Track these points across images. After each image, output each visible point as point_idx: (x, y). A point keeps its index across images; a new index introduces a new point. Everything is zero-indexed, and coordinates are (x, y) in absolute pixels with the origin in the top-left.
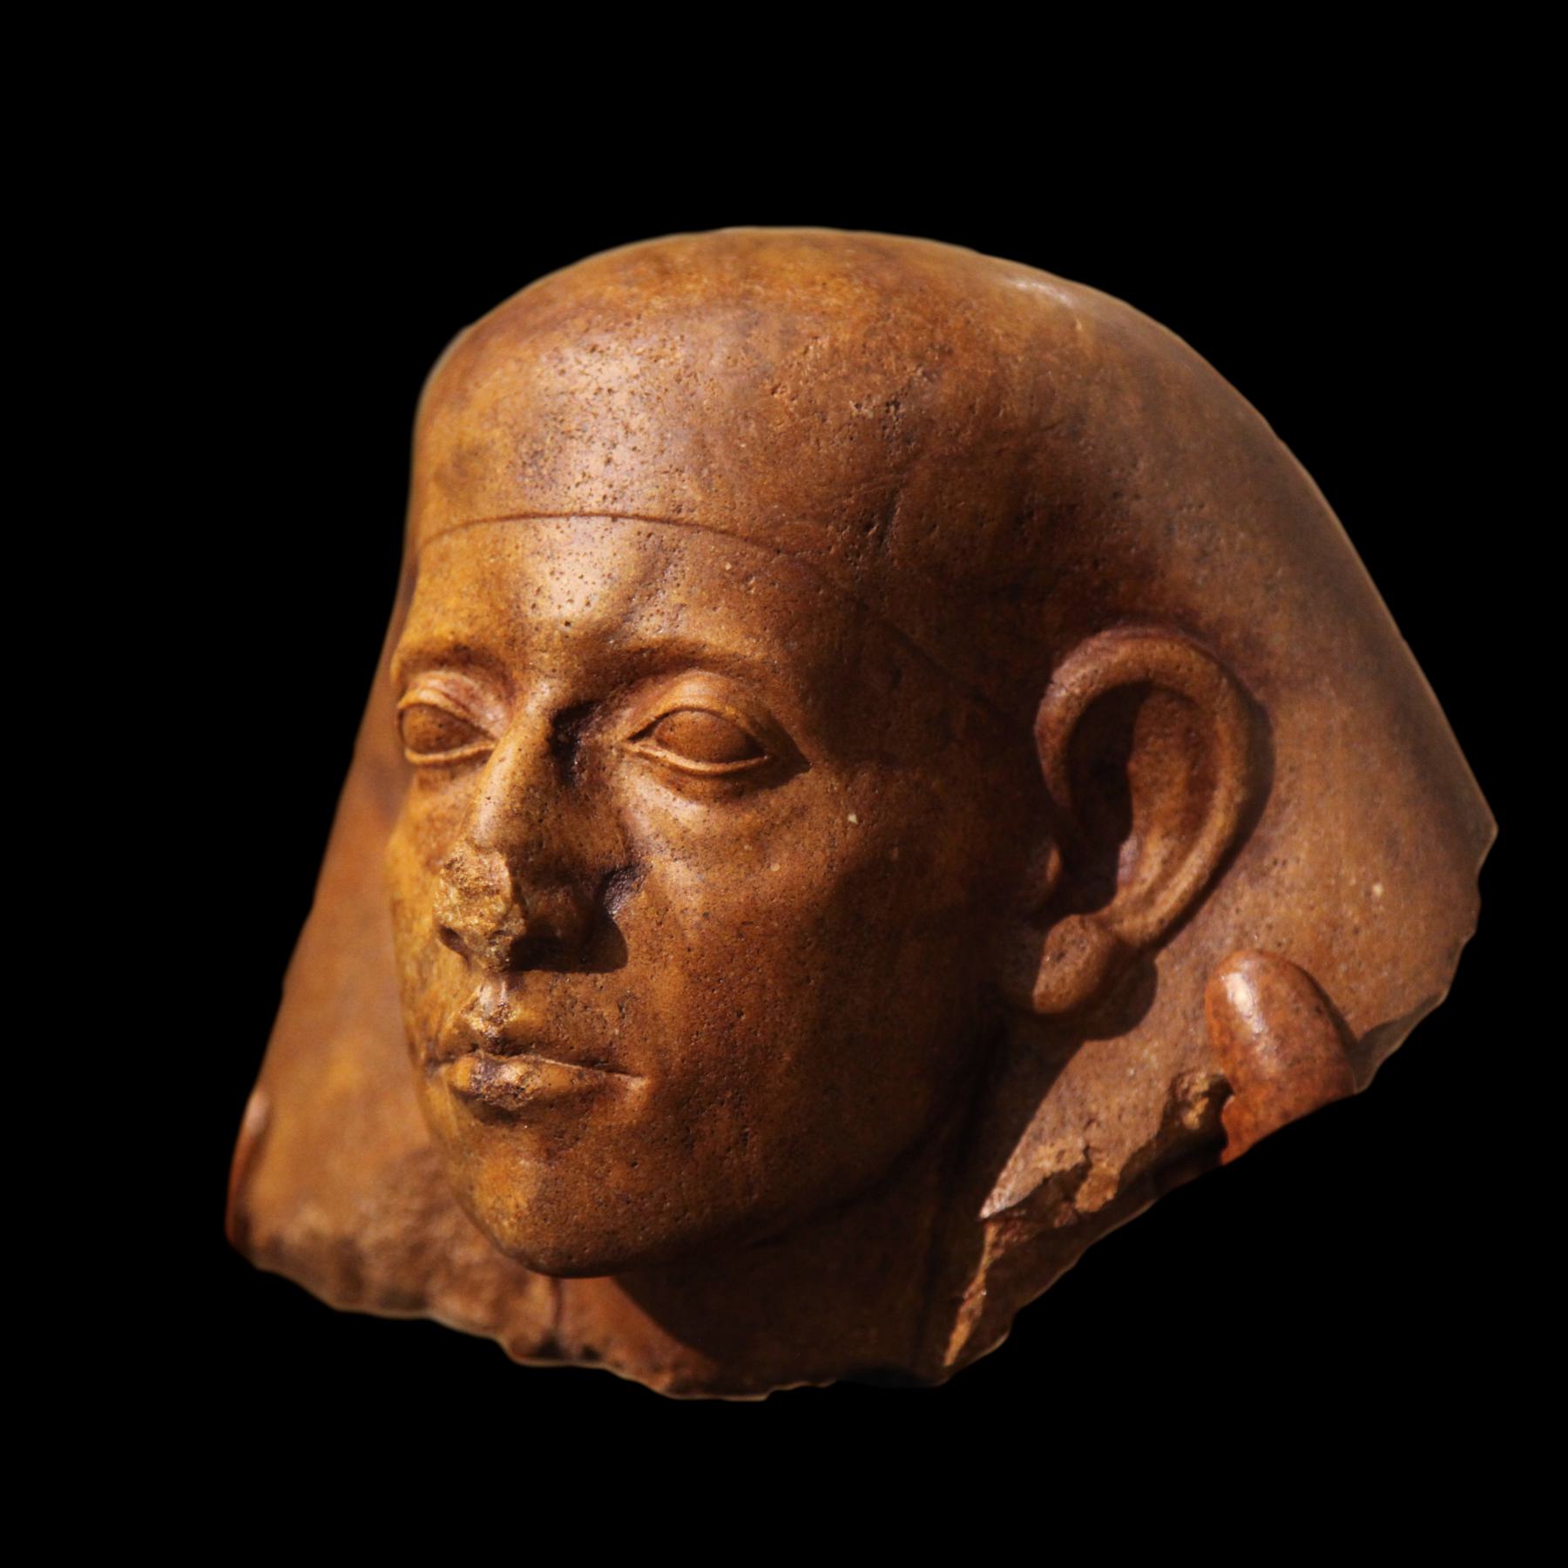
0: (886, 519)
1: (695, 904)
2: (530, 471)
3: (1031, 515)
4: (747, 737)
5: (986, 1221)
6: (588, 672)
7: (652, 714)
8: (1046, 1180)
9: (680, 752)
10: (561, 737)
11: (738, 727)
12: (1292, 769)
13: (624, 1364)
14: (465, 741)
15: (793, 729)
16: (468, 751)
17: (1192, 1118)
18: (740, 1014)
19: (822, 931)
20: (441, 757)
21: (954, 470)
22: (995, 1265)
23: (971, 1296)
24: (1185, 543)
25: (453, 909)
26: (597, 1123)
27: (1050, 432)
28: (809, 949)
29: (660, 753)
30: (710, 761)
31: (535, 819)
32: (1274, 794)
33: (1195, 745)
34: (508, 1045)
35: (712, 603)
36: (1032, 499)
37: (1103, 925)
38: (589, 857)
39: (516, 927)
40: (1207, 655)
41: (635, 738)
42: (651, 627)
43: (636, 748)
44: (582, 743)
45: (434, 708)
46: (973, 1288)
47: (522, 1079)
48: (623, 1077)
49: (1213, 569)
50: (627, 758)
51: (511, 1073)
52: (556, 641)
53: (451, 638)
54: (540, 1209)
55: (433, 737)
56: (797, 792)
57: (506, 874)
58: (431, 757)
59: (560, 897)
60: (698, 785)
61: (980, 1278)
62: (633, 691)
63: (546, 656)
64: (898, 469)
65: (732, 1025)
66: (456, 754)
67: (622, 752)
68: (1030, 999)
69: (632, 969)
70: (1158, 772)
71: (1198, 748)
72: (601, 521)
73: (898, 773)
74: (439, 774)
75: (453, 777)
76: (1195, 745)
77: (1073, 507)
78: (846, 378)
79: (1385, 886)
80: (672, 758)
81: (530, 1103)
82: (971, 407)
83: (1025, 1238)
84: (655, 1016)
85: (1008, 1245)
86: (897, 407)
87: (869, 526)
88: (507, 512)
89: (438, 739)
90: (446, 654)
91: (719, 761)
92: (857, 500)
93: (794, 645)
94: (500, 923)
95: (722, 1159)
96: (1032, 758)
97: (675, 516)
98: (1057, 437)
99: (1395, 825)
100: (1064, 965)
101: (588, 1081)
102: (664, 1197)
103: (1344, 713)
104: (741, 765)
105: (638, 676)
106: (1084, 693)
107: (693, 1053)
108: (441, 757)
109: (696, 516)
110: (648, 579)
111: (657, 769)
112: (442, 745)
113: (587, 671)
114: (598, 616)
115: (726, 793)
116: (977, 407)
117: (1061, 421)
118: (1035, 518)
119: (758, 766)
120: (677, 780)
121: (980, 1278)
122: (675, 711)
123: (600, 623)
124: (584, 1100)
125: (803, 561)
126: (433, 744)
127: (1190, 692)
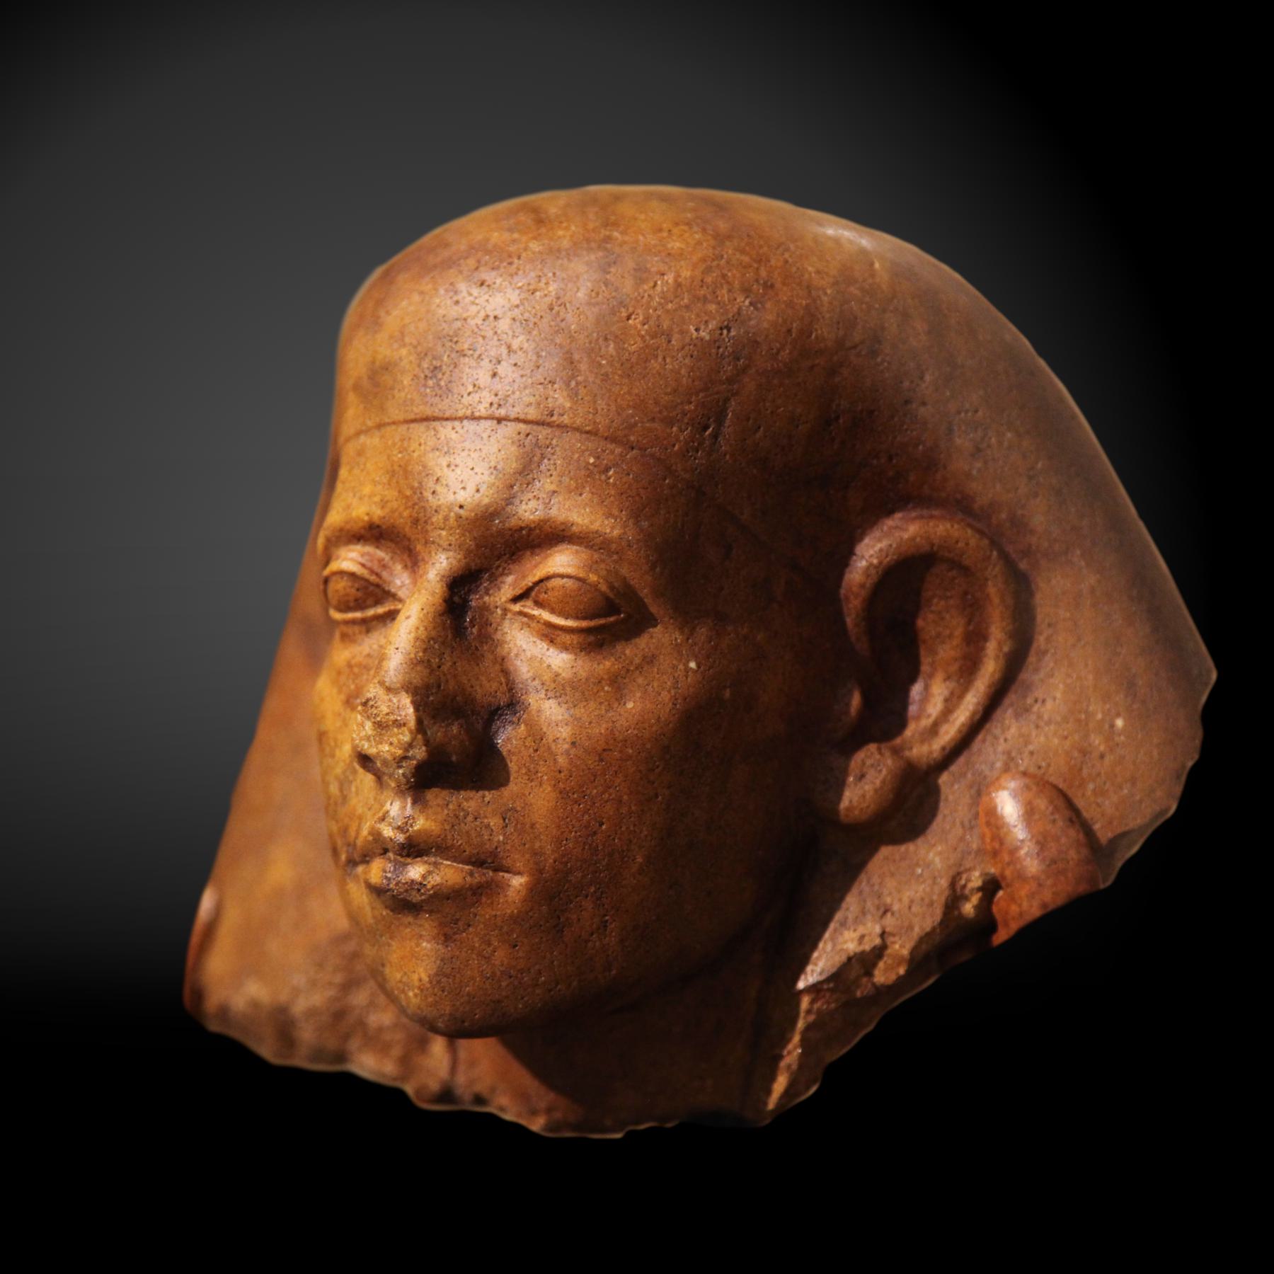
0: (720, 422)
1: (564, 735)
2: (430, 383)
3: (837, 418)
4: (607, 599)
5: (801, 992)
6: (478, 546)
7: (530, 580)
8: (850, 959)
9: (553, 611)
10: (456, 599)
11: (600, 591)
12: (1049, 625)
13: (507, 1108)
14: (378, 602)
15: (645, 593)
16: (380, 610)
17: (968, 908)
18: (601, 824)
19: (668, 757)
20: (358, 615)
21: (775, 382)
22: (808, 1028)
23: (789, 1053)
24: (962, 441)
25: (368, 738)
26: (485, 912)
27: (853, 351)
28: (657, 771)
29: (536, 612)
30: (577, 618)
31: (434, 666)
32: (1035, 645)
33: (971, 606)
34: (413, 849)
35: (579, 490)
36: (839, 405)
37: (896, 752)
38: (479, 697)
39: (420, 753)
40: (981, 533)
41: (516, 599)
42: (529, 510)
43: (517, 607)
44: (473, 604)
45: (352, 575)
46: (790, 1046)
47: (424, 877)
48: (506, 875)
49: (986, 463)
50: (509, 616)
51: (415, 871)
52: (452, 521)
53: (366, 518)
54: (439, 982)
55: (351, 599)
56: (647, 644)
57: (411, 710)
58: (350, 615)
59: (455, 729)
60: (567, 638)
61: (797, 1038)
62: (514, 562)
63: (444, 533)
64: (730, 381)
65: (595, 833)
66: (371, 612)
67: (505, 611)
68: (837, 812)
69: (513, 787)
70: (941, 627)
71: (973, 608)
72: (488, 424)
73: (730, 628)
74: (356, 629)
75: (368, 631)
76: (971, 606)
77: (872, 412)
78: (687, 307)
79: (1125, 720)
80: (546, 616)
81: (431, 896)
82: (789, 331)
83: (833, 1005)
84: (533, 826)
85: (819, 1012)
86: (729, 331)
87: (706, 428)
88: (412, 416)
89: (356, 600)
90: (363, 532)
91: (584, 618)
92: (696, 406)
93: (645, 524)
94: (406, 750)
95: (587, 941)
96: (839, 616)
97: (549, 419)
98: (858, 355)
99: (1134, 671)
100: (864, 784)
101: (477, 878)
102: (540, 972)
103: (1092, 579)
104: (602, 621)
105: (519, 549)
106: (880, 563)
107: (563, 856)
108: (358, 615)
109: (566, 419)
110: (526, 470)
111: (534, 624)
112: (359, 605)
113: (477, 545)
114: (486, 501)
115: (590, 644)
116: (794, 331)
117: (862, 342)
118: (841, 421)
119: (616, 623)
120: (550, 634)
121: (797, 1038)
122: (548, 578)
123: (487, 506)
124: (474, 894)
125: (652, 456)
126: (352, 604)
127: (967, 562)
